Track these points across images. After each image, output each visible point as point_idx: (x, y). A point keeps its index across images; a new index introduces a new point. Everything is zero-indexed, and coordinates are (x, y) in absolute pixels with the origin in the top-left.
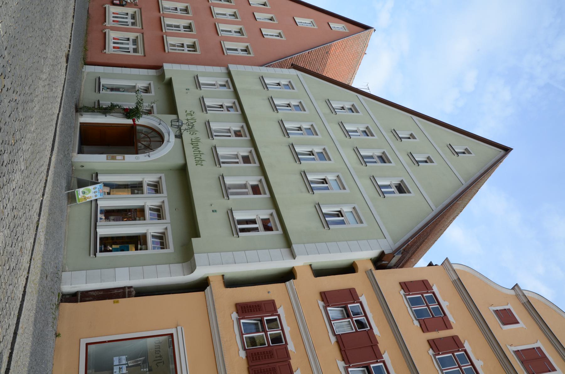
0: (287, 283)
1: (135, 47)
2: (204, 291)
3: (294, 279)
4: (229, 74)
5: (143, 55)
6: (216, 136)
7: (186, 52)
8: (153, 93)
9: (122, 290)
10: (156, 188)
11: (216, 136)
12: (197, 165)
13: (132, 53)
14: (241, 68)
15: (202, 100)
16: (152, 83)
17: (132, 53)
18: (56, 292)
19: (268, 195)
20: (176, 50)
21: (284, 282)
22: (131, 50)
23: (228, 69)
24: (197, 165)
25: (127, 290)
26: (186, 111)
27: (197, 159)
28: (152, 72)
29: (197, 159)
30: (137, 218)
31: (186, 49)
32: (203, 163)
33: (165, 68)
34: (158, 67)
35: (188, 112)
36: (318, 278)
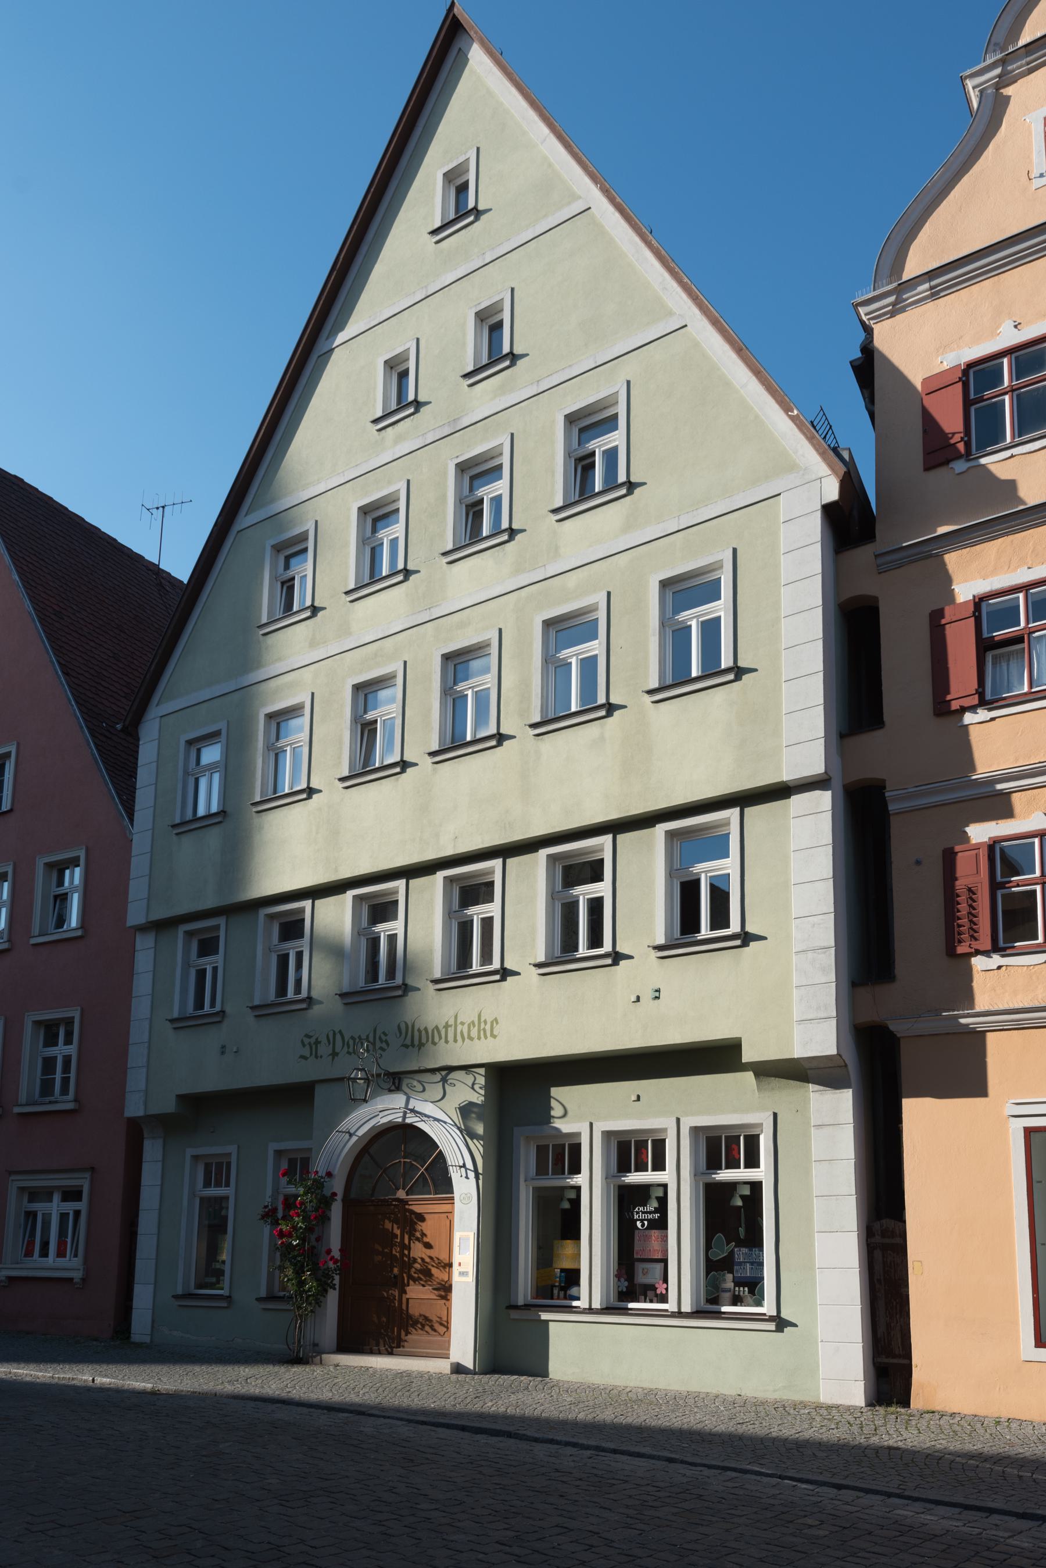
0: (892, 807)
1: (56, 1197)
2: (899, 1039)
3: (885, 788)
4: (162, 926)
5: (88, 1175)
6: (213, 1004)
7: (72, 1050)
8: (232, 1149)
9: (878, 1254)
10: (216, 1171)
11: (213, 1004)
12: (494, 1036)
13: (82, 1206)
14: (137, 889)
15: (263, 1012)
16: (190, 1152)
17: (82, 1206)
18: (868, 1414)
19: (221, 921)
20: (65, 1081)
21: (889, 815)
22: (70, 1207)
23: (143, 929)
24: (494, 1036)
25: (877, 1239)
26: (303, 1057)
27: (474, 1032)
28: (152, 1150)
29: (474, 1032)
30: (223, 1213)
31: (60, 1050)
32: (488, 1016)
33: (141, 1113)
34: (135, 1132)
35: (306, 1052)
36: (885, 718)
